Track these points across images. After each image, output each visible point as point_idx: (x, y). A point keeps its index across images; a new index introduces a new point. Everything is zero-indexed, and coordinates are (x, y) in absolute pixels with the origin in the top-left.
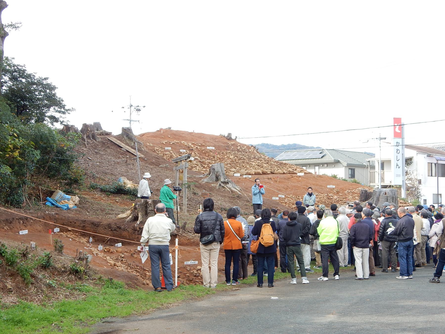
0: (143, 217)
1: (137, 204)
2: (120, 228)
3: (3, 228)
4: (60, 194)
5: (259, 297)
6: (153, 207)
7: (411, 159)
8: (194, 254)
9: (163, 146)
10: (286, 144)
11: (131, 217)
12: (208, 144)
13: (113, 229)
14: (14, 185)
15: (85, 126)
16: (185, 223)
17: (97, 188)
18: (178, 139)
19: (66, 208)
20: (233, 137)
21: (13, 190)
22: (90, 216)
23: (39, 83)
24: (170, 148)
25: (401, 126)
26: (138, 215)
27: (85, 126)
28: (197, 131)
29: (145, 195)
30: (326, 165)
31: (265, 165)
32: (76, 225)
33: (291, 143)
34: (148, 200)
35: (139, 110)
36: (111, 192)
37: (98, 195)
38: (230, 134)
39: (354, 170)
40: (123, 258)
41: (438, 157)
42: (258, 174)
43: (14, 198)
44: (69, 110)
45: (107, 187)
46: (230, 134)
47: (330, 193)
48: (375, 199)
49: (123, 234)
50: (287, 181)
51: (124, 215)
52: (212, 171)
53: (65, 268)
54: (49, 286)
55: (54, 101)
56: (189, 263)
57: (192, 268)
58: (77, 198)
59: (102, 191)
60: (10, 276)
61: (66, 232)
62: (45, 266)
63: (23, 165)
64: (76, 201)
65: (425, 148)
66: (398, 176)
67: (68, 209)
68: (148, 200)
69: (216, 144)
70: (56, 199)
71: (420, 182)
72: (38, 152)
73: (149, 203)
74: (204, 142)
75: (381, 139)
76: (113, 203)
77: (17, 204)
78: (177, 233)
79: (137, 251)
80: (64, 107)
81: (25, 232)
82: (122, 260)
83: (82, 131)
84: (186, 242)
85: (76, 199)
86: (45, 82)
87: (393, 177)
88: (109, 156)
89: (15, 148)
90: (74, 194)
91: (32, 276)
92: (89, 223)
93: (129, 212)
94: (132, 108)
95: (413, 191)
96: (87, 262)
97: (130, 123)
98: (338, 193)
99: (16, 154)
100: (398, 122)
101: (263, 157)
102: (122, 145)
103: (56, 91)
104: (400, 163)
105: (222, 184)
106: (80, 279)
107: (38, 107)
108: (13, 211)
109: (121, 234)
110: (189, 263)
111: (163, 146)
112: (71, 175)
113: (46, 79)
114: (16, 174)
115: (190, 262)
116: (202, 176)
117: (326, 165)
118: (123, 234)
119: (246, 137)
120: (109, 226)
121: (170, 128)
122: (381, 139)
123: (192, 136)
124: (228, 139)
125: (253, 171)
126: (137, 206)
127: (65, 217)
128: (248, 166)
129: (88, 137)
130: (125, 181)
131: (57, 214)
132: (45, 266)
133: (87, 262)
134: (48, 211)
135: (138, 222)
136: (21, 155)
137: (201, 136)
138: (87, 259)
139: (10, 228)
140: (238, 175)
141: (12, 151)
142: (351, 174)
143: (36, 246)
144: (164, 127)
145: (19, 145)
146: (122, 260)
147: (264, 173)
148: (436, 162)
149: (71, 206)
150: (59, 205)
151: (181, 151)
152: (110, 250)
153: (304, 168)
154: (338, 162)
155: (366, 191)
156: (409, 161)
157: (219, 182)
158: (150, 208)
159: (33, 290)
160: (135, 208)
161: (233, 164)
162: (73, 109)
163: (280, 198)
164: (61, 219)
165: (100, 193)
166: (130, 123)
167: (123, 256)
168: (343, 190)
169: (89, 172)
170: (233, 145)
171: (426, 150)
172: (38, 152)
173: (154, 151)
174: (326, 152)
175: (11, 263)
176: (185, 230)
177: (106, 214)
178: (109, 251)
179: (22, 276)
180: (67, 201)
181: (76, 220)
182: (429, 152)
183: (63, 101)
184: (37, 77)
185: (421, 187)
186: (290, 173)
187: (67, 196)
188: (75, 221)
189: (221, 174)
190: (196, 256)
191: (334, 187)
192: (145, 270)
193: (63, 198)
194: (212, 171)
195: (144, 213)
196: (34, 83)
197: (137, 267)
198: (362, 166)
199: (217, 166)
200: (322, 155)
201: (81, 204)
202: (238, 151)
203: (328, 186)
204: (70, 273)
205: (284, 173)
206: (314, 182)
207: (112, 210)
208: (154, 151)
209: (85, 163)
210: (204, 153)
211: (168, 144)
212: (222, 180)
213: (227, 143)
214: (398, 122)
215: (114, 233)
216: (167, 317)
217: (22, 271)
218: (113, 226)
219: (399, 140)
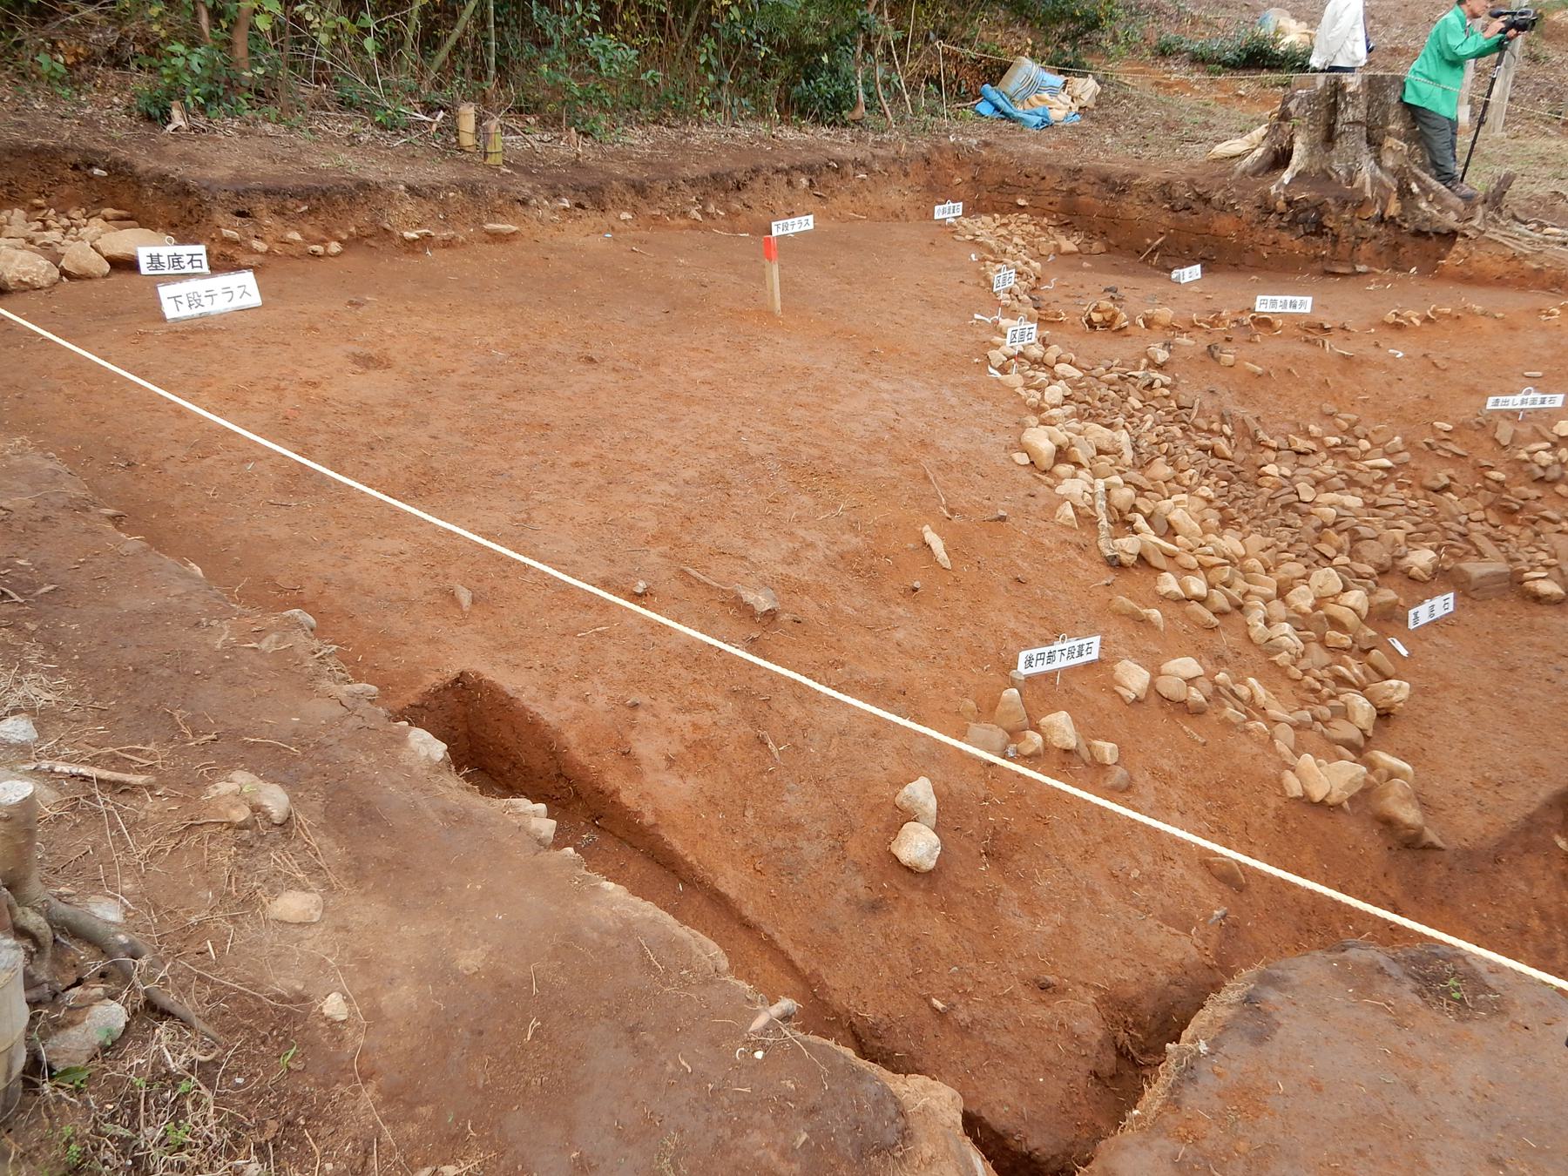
0: (1311, 154)
1: (1292, 97)
2: (1208, 201)
3: (684, 214)
4: (1027, 70)
6: (1363, 107)
8: (1539, 339)
11: (1259, 152)
13: (1179, 205)
16: (1507, 181)
17: (1179, 52)
19: (1037, 120)
22: (1111, 153)
26: (1291, 142)
29: (1340, 63)
32: (1044, 185)
34: (1346, 78)
36: (1225, 64)
37: (1178, 72)
40: (1160, 367)
49: (1217, 225)
51: (1235, 146)
57: (1525, 430)
59: (1200, 60)
61: (1003, 214)
64: (1086, 97)
67: (1047, 124)
68: (1346, 78)
70: (1010, 91)
73: (1350, 89)
76: (1225, 102)
78: (1457, 226)
79: (1247, 319)
81: (803, 224)
82: (1150, 386)
84: (1500, 269)
85: (1087, 88)
92: (1092, 180)
109: (1207, 226)
110: (1514, 402)
115: (1518, 398)
118: (1217, 225)
126: (1292, 106)
127: (1011, 155)
130: (1282, 23)
131: (986, 144)
135: (1286, 176)
139: (728, 211)
146: (1150, 386)
149: (1056, 114)
150: (1019, 111)
152: (1114, 316)
158: (1350, 114)
160: (1285, 116)
165: (1186, 69)
176: (1500, 211)
177: (1182, 140)
180: (1046, 95)
181: (1049, 166)
187: (1058, 80)
188: (1044, 173)
190: (1547, 353)
192: (1259, 443)
193: (1035, 87)
195: (1319, 135)
196: (1437, 956)
197: (1223, 422)
201: (1095, 114)
207: (1206, 126)
215: (1180, 220)
218: (1182, 192)
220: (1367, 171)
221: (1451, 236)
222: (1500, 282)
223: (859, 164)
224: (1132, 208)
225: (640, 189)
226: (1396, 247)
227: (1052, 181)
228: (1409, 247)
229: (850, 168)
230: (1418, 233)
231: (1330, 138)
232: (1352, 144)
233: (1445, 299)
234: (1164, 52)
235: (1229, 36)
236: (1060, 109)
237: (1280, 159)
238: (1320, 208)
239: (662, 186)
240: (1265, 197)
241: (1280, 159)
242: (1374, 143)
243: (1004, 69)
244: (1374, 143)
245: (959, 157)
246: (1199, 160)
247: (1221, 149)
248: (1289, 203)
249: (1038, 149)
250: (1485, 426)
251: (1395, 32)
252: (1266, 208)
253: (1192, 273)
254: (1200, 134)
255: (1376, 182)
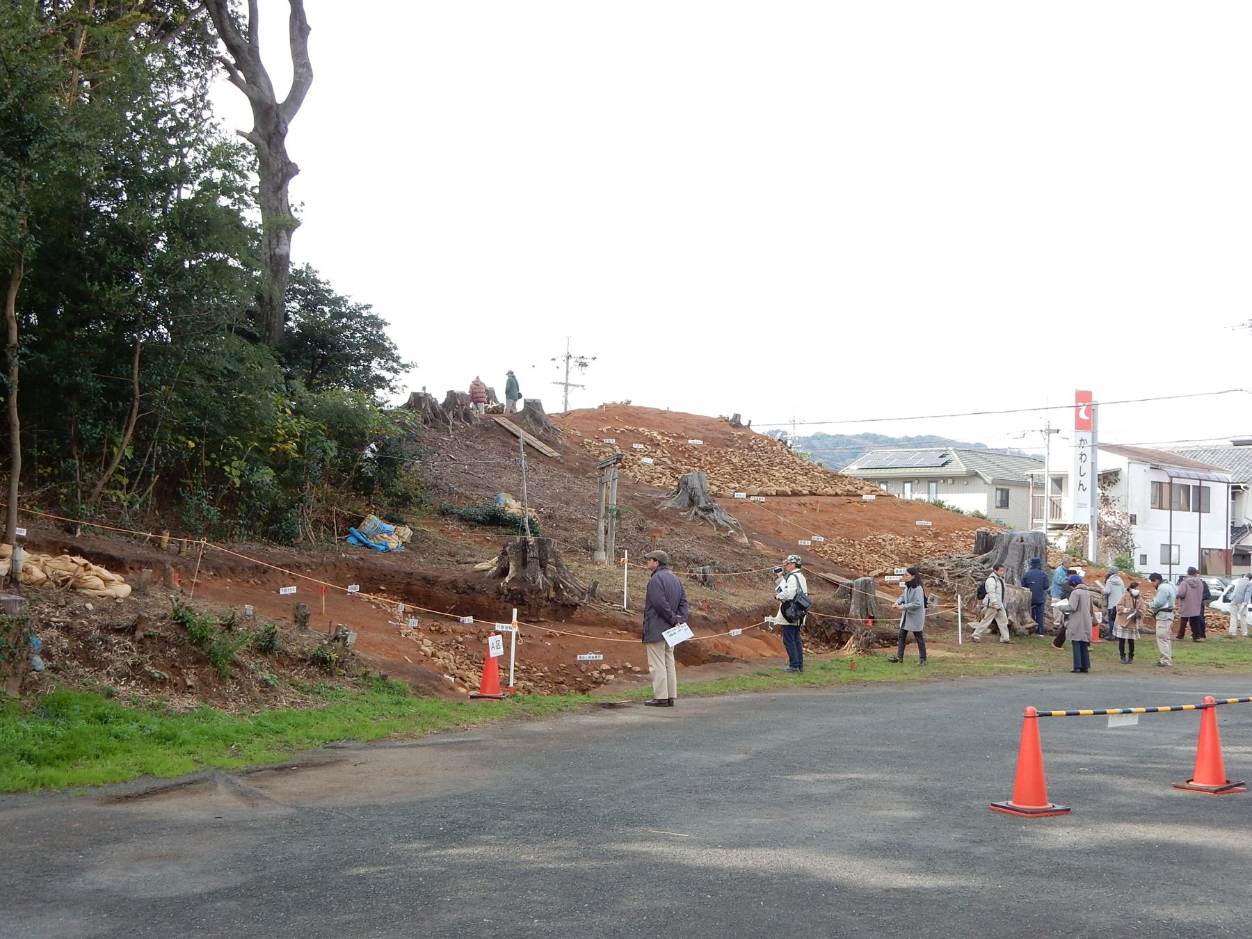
4: (373, 521)
5: (652, 719)
7: (1116, 473)
9: (599, 436)
10: (912, 435)
12: (691, 434)
14: (281, 504)
15: (451, 395)
16: (596, 584)
18: (634, 423)
19: (382, 548)
20: (744, 422)
21: (276, 514)
22: (422, 565)
23: (353, 315)
24: (613, 441)
25: (1091, 411)
27: (451, 395)
28: (674, 409)
30: (950, 481)
31: (800, 478)
33: (924, 433)
35: (583, 365)
36: (478, 522)
37: (452, 525)
38: (737, 416)
39: (1007, 491)
41: (1174, 470)
42: (784, 494)
43: (280, 528)
44: (407, 366)
45: (472, 511)
46: (737, 416)
47: (920, 535)
48: (1000, 550)
50: (836, 510)
51: (485, 565)
52: (682, 486)
53: (303, 653)
54: (265, 683)
55: (379, 348)
56: (586, 657)
58: (408, 530)
60: (195, 663)
62: (266, 647)
63: (301, 467)
65: (1152, 451)
66: (1080, 505)
67: (388, 550)
69: (708, 434)
71: (1133, 520)
72: (333, 444)
74: (686, 429)
75: (1049, 432)
77: (286, 538)
80: (396, 360)
81: (292, 590)
83: (444, 405)
84: (594, 619)
85: (406, 532)
86: (365, 313)
87: (1076, 507)
88: (491, 451)
89: (291, 435)
90: (403, 524)
91: (235, 664)
93: (496, 559)
94: (571, 361)
95: (1117, 539)
96: (344, 645)
97: (566, 390)
98: (936, 535)
99: (291, 446)
100: (1084, 397)
101: (799, 462)
102: (521, 433)
103: (385, 330)
104: (1087, 481)
105: (700, 513)
106: (330, 674)
107: (349, 359)
108: (277, 550)
110: (586, 657)
111: (599, 436)
112: (399, 485)
113: (367, 307)
114: (285, 484)
116: (663, 496)
117: (950, 481)
119: (761, 422)
120: (454, 584)
121: (629, 402)
122: (1049, 432)
123: (662, 419)
124: (734, 426)
125: (773, 489)
128: (765, 480)
129: (456, 416)
132: (266, 647)
133: (344, 645)
134: (346, 552)
135: (507, 579)
136: (300, 450)
137: (682, 418)
138: (346, 638)
140: (743, 495)
141: (285, 442)
142: (1002, 501)
143: (255, 613)
144: (609, 402)
145: (297, 430)
147: (795, 494)
148: (1197, 483)
149: (392, 545)
150: (372, 542)
151: (635, 446)
153: (883, 487)
154: (976, 475)
155: (987, 534)
156: (1109, 478)
157: (695, 509)
159: (233, 688)
160: (504, 553)
161: (739, 473)
162: (414, 365)
163: (814, 542)
164: (369, 569)
166: (566, 390)
167: (461, 639)
168: (949, 530)
169: (442, 483)
170: (740, 437)
171: (1151, 457)
172: (333, 444)
173: (583, 447)
174: (952, 454)
175: (201, 641)
178: (438, 631)
179: (214, 664)
182: (1154, 460)
183: (395, 348)
184: (351, 303)
185: (1135, 529)
186: (849, 494)
187: (391, 527)
189: (700, 494)
191: (930, 524)
194: (682, 486)
195: (520, 562)
196: (342, 315)
198: (1024, 485)
199: (694, 477)
200: (944, 460)
201: (413, 545)
202: (750, 448)
203: (918, 523)
204: (313, 664)
205: (837, 495)
206: (891, 514)
208: (583, 447)
209: (441, 465)
210: (681, 452)
211: (610, 434)
212: (702, 505)
213: (728, 435)
214: (1084, 397)
216: (444, 744)
217: (216, 655)
218: (461, 584)
219: (1087, 435)
220: (540, 578)
221: (575, 606)
222: (593, 624)
223: (307, 565)
224: (438, 592)
225: (232, 570)
226: (556, 611)
227: (398, 578)
228: (561, 612)
229: (303, 567)
230: (564, 605)
231: (525, 564)
232: (534, 565)
233: (568, 630)
234: (443, 513)
235: (479, 504)
236: (394, 543)
237: (504, 572)
238: (522, 593)
239: (239, 569)
240: (498, 587)
241: (504, 572)
242: (543, 566)
243: (361, 520)
244: (543, 566)
245: (348, 565)
246: (468, 571)
247: (477, 566)
248: (509, 590)
249: (388, 562)
250: (577, 665)
251: (572, 509)
252: (499, 592)
253: (469, 620)
254: (469, 559)
255: (544, 583)
